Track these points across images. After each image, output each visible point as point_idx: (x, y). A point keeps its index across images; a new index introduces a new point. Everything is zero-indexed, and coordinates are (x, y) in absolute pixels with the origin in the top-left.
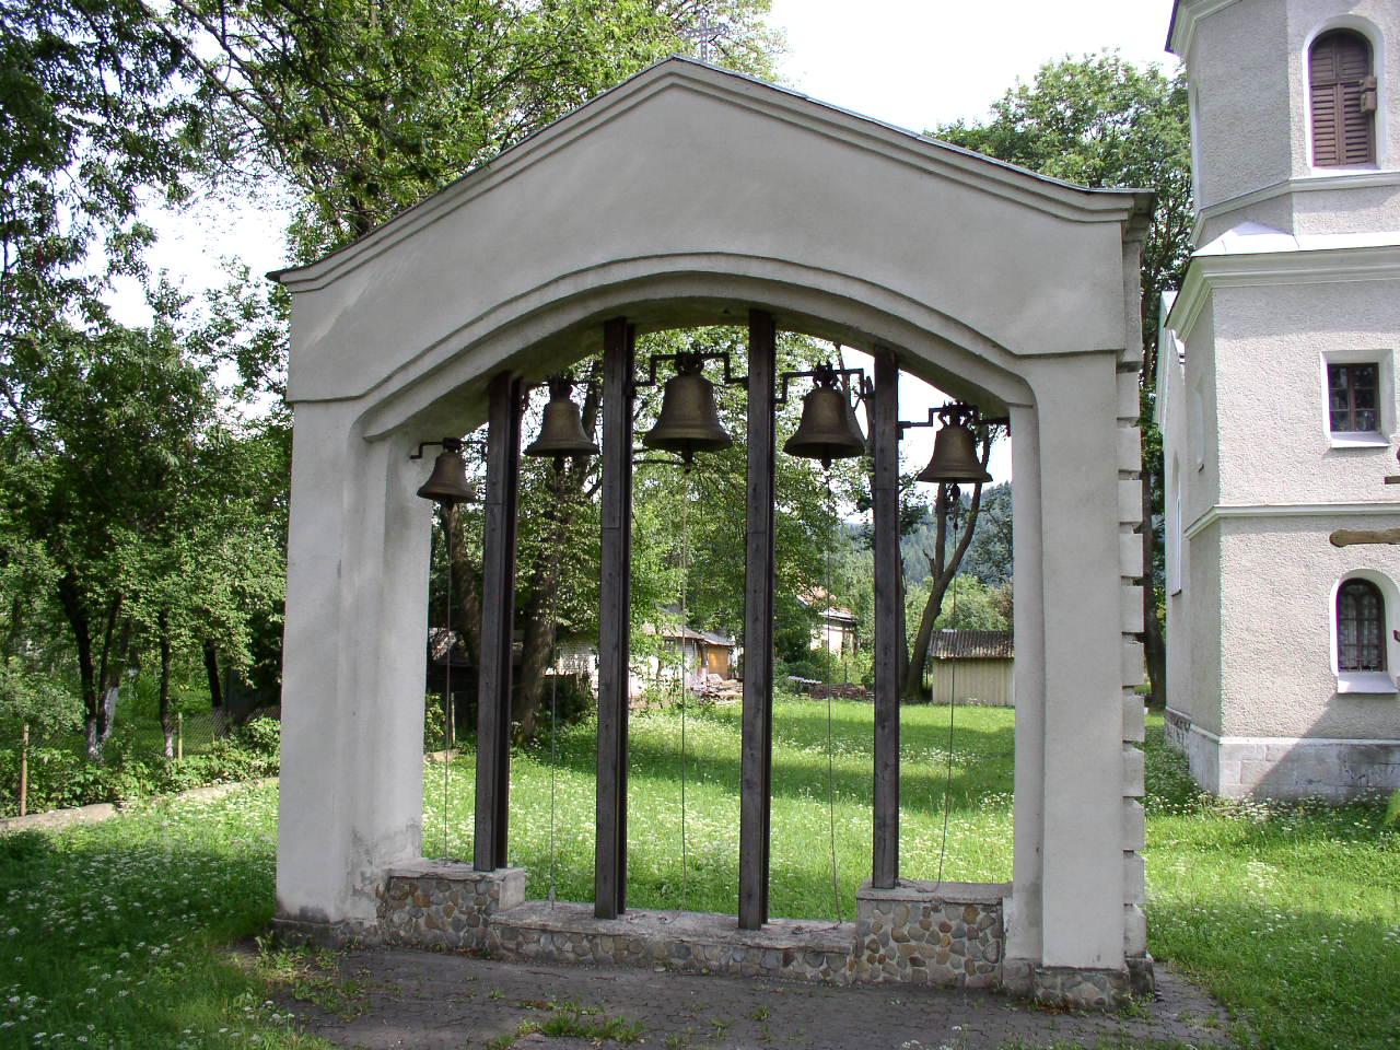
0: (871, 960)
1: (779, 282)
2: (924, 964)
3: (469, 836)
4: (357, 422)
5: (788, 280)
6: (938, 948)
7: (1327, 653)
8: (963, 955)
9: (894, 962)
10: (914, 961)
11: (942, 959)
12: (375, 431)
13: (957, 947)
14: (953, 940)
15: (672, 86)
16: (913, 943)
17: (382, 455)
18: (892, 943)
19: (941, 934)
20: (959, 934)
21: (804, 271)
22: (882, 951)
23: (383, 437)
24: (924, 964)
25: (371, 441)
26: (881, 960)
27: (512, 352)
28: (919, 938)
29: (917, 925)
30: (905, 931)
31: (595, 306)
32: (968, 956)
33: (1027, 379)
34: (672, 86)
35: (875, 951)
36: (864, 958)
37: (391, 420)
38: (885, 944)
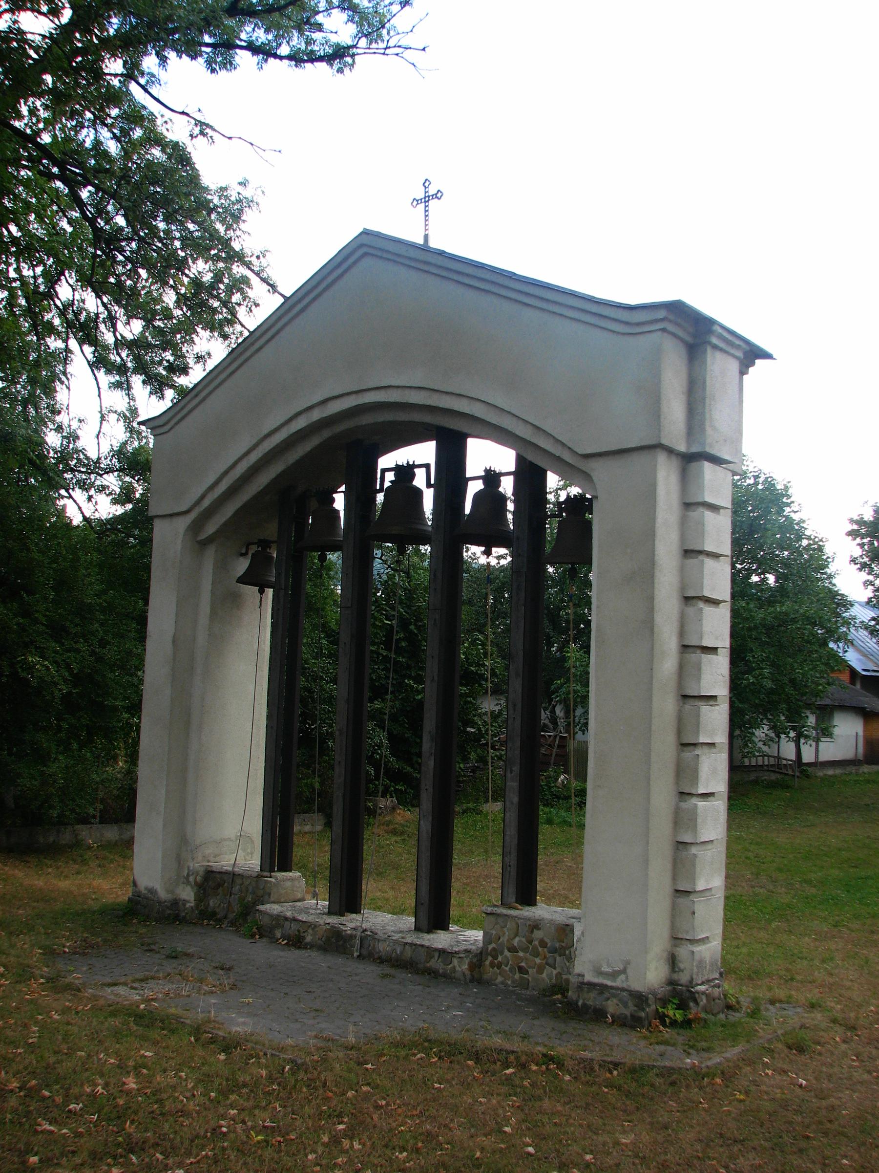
0: (492, 965)
1: (429, 406)
2: (527, 973)
3: (549, 822)
4: (189, 527)
5: (433, 404)
6: (538, 961)
7: (596, 642)
8: (555, 968)
9: (507, 969)
10: (521, 970)
11: (540, 970)
12: (203, 536)
13: (551, 961)
14: (548, 955)
15: (366, 254)
16: (521, 954)
17: (210, 556)
18: (506, 953)
19: (540, 949)
20: (554, 951)
21: (444, 396)
22: (500, 959)
23: (210, 540)
24: (527, 973)
25: (204, 544)
26: (499, 966)
27: (278, 473)
28: (525, 950)
29: (524, 940)
30: (516, 942)
31: (326, 434)
32: (558, 970)
33: (592, 474)
34: (366, 254)
35: (495, 957)
36: (487, 963)
37: (211, 528)
38: (502, 953)
